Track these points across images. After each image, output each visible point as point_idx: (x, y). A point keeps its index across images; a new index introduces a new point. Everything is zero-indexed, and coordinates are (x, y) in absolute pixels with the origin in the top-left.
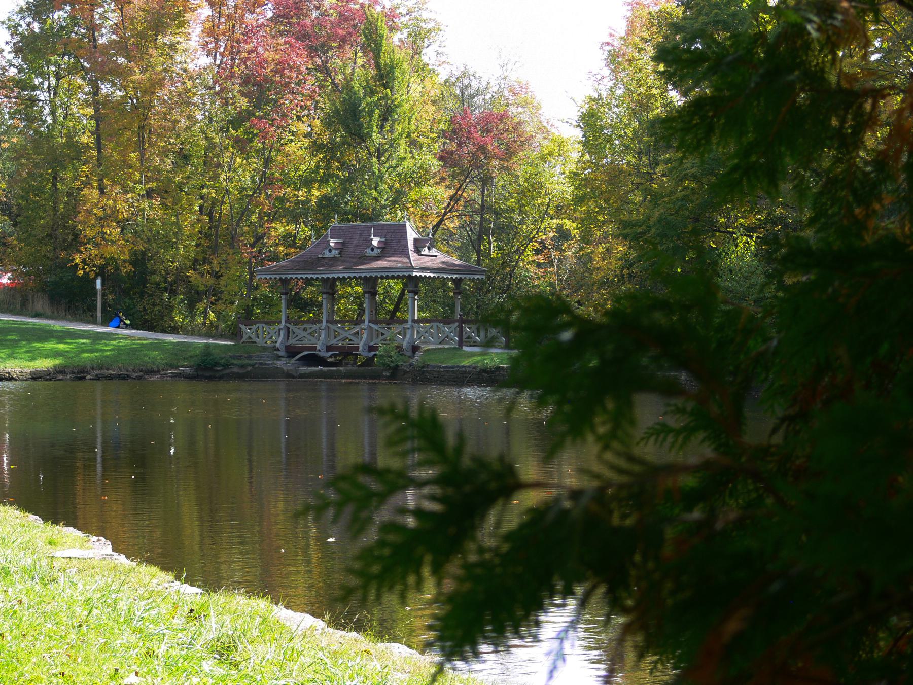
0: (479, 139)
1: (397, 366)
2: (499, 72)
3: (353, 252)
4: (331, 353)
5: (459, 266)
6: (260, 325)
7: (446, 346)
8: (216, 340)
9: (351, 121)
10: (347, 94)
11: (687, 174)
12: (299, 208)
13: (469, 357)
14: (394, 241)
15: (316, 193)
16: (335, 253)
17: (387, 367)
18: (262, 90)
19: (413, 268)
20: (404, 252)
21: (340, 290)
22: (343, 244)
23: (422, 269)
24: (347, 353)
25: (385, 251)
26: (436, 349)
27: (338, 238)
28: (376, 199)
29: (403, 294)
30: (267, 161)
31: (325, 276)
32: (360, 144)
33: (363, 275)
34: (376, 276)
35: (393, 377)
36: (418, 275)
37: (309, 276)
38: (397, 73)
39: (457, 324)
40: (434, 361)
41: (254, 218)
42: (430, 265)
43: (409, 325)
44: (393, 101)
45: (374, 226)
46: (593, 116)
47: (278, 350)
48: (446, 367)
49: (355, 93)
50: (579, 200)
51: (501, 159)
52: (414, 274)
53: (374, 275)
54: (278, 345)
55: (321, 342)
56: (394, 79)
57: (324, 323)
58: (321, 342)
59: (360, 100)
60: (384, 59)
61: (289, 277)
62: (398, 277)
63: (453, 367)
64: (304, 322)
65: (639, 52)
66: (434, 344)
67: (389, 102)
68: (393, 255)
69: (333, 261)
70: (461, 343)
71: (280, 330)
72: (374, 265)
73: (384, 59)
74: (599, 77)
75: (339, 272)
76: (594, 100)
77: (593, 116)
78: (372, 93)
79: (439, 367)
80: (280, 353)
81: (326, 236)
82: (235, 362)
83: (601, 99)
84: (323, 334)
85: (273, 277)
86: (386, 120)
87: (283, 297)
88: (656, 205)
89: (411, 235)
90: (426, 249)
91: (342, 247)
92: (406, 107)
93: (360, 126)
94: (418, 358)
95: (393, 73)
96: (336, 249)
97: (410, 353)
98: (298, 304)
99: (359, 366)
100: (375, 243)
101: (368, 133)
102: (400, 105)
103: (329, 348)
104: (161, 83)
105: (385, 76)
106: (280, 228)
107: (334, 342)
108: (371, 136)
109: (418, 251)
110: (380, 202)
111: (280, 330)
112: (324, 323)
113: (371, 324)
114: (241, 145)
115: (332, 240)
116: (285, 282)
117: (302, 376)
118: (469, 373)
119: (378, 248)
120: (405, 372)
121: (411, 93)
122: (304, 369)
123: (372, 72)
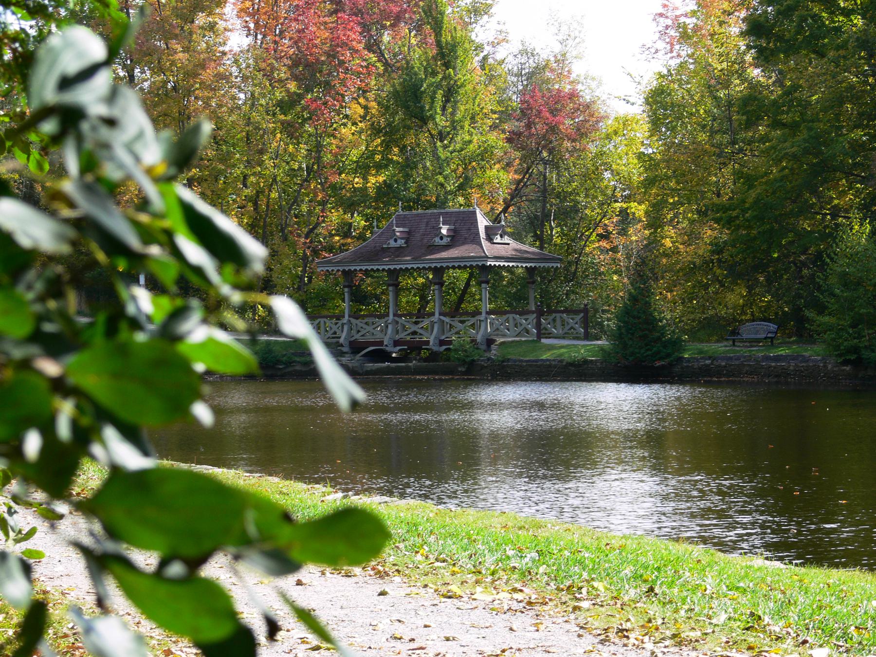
0: (545, 118)
1: (473, 361)
2: (558, 48)
3: (421, 242)
4: (444, 347)
5: (533, 253)
6: (322, 320)
7: (523, 339)
8: (271, 336)
9: (413, 103)
10: (407, 75)
11: (787, 154)
12: (356, 196)
13: (549, 350)
14: (464, 227)
15: (373, 180)
16: (401, 242)
17: (464, 362)
18: (313, 72)
19: (487, 257)
20: (476, 240)
21: (406, 282)
22: (409, 233)
23: (497, 258)
24: (414, 347)
25: (455, 239)
26: (513, 342)
27: (403, 227)
28: (442, 185)
29: (468, 285)
30: (319, 147)
31: (392, 267)
32: (421, 127)
33: (433, 266)
34: (355, 270)
35: (468, 372)
36: (493, 264)
37: (369, 268)
38: (460, 52)
39: (535, 315)
40: (514, 354)
41: (304, 208)
42: (503, 253)
43: (482, 317)
44: (456, 81)
45: (441, 213)
46: (663, 92)
47: (342, 345)
48: (529, 361)
49: (416, 74)
50: (649, 183)
51: (574, 141)
52: (489, 263)
53: (444, 265)
54: (341, 340)
55: (388, 336)
56: (457, 58)
57: (347, 317)
58: (388, 336)
59: (422, 81)
60: (446, 37)
61: (353, 268)
62: (465, 267)
63: (534, 361)
64: (364, 316)
65: (721, 25)
66: (510, 337)
67: (452, 82)
68: (463, 244)
69: (399, 252)
70: (540, 336)
71: (343, 325)
72: (444, 255)
73: (446, 37)
74: (653, 51)
75: (407, 262)
76: (663, 76)
77: (663, 92)
78: (434, 74)
79: (522, 361)
80: (345, 349)
81: (391, 225)
82: (298, 359)
83: (671, 75)
84: (346, 328)
85: (335, 269)
86: (448, 101)
87: (346, 290)
88: (751, 186)
89: (482, 222)
90: (498, 236)
91: (408, 236)
92: (469, 87)
93: (422, 108)
94: (494, 352)
95: (456, 52)
96: (402, 238)
97: (484, 347)
98: (359, 297)
99: (426, 360)
100: (444, 231)
101: (431, 115)
102: (463, 85)
103: (396, 343)
104: (203, 66)
105: (447, 55)
106: (335, 217)
107: (402, 335)
108: (434, 119)
109: (490, 239)
110: (445, 188)
111: (343, 325)
112: (347, 317)
113: (442, 317)
114: (291, 131)
115: (397, 229)
116: (347, 274)
117: (368, 373)
118: (555, 366)
119: (448, 236)
120: (483, 367)
121: (469, 71)
122: (370, 366)
123: (432, 52)
